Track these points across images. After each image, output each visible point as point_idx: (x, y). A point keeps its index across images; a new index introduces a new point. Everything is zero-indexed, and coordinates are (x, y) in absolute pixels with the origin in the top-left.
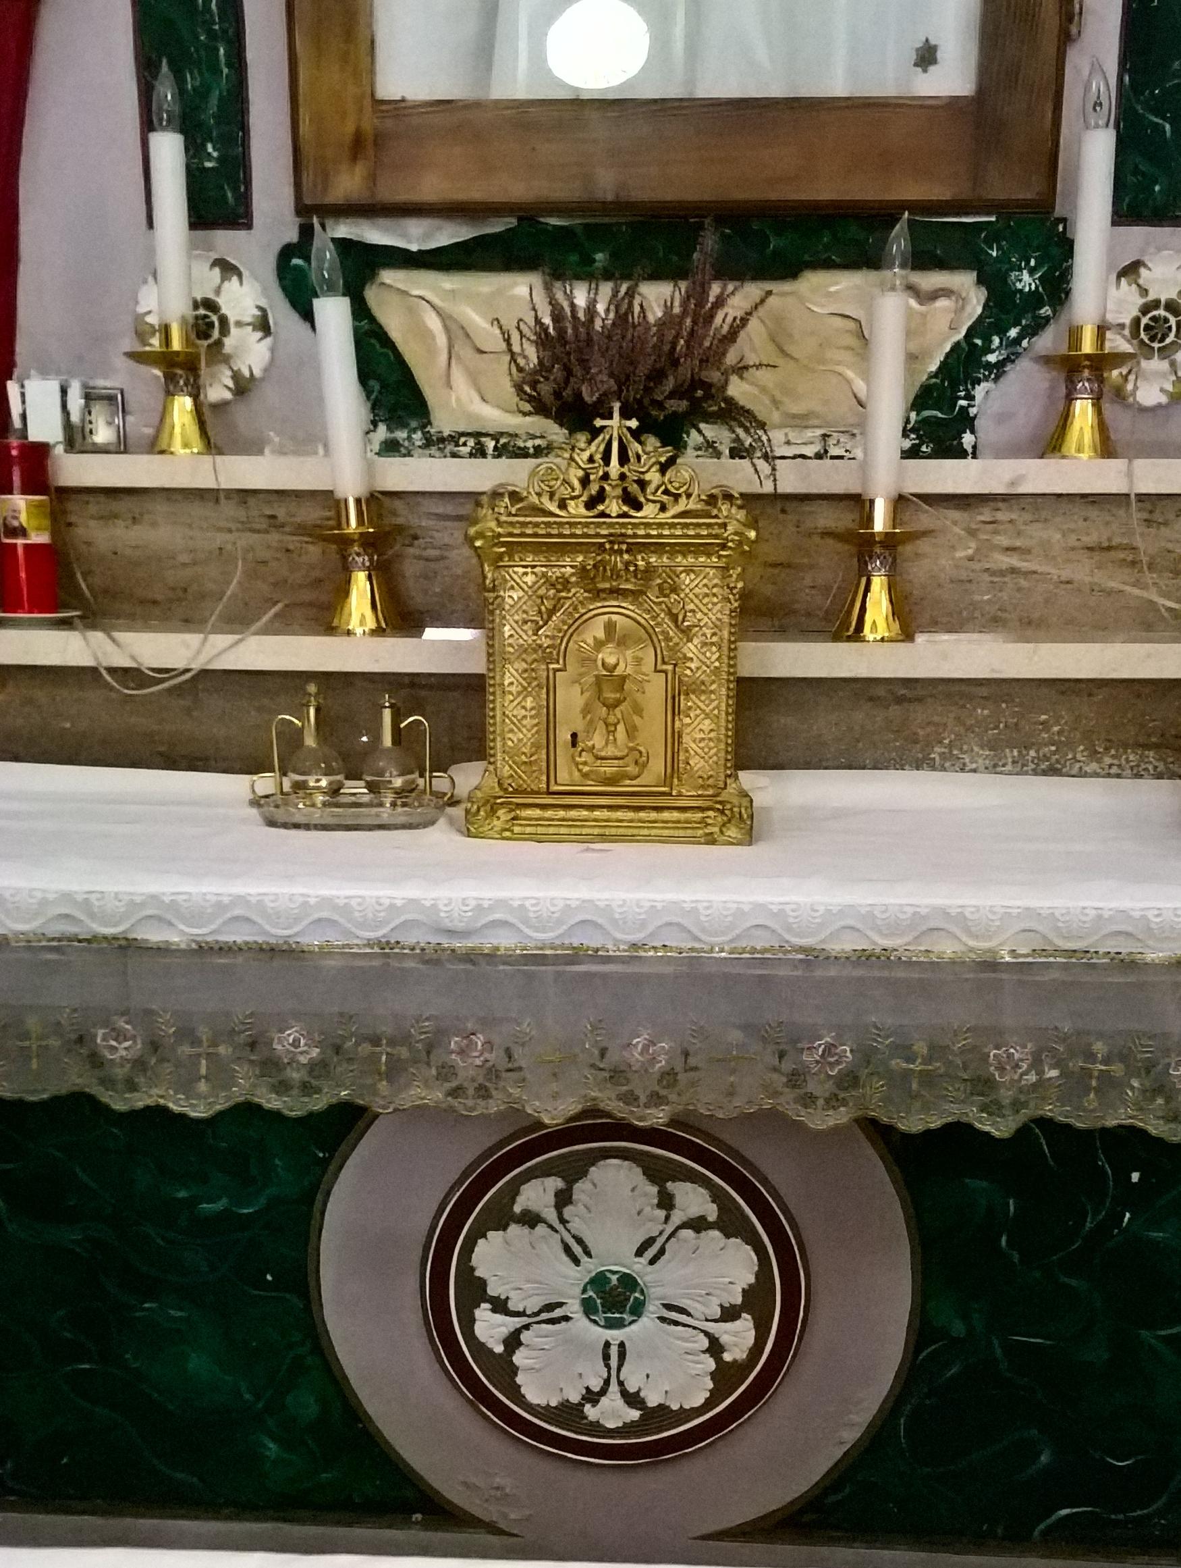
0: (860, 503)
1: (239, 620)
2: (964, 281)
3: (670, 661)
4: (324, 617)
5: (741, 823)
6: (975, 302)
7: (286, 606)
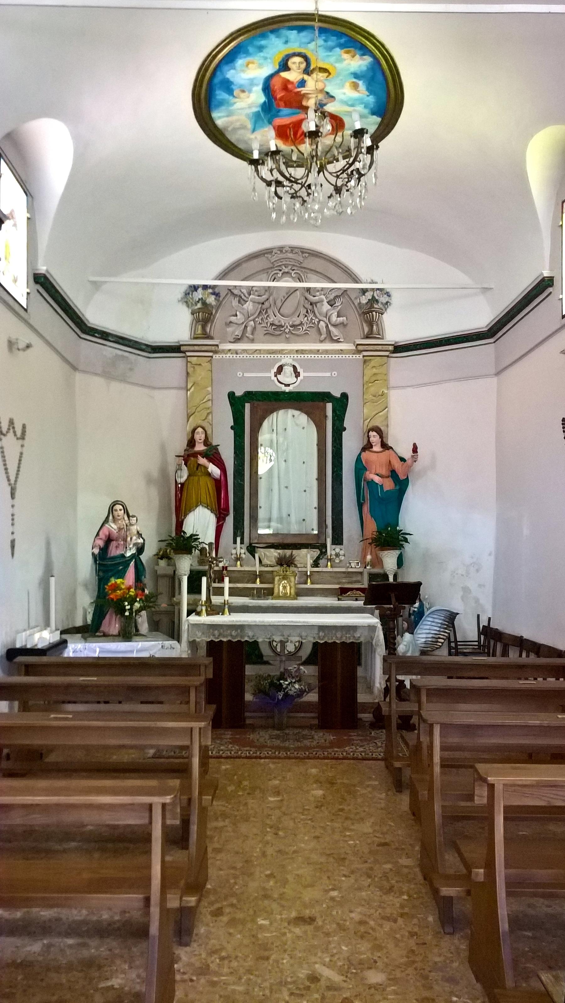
0: (386, 576)
1: (247, 582)
2: (318, 550)
3: (290, 585)
4: (254, 582)
5: (297, 599)
6: (319, 552)
7: (186, 464)
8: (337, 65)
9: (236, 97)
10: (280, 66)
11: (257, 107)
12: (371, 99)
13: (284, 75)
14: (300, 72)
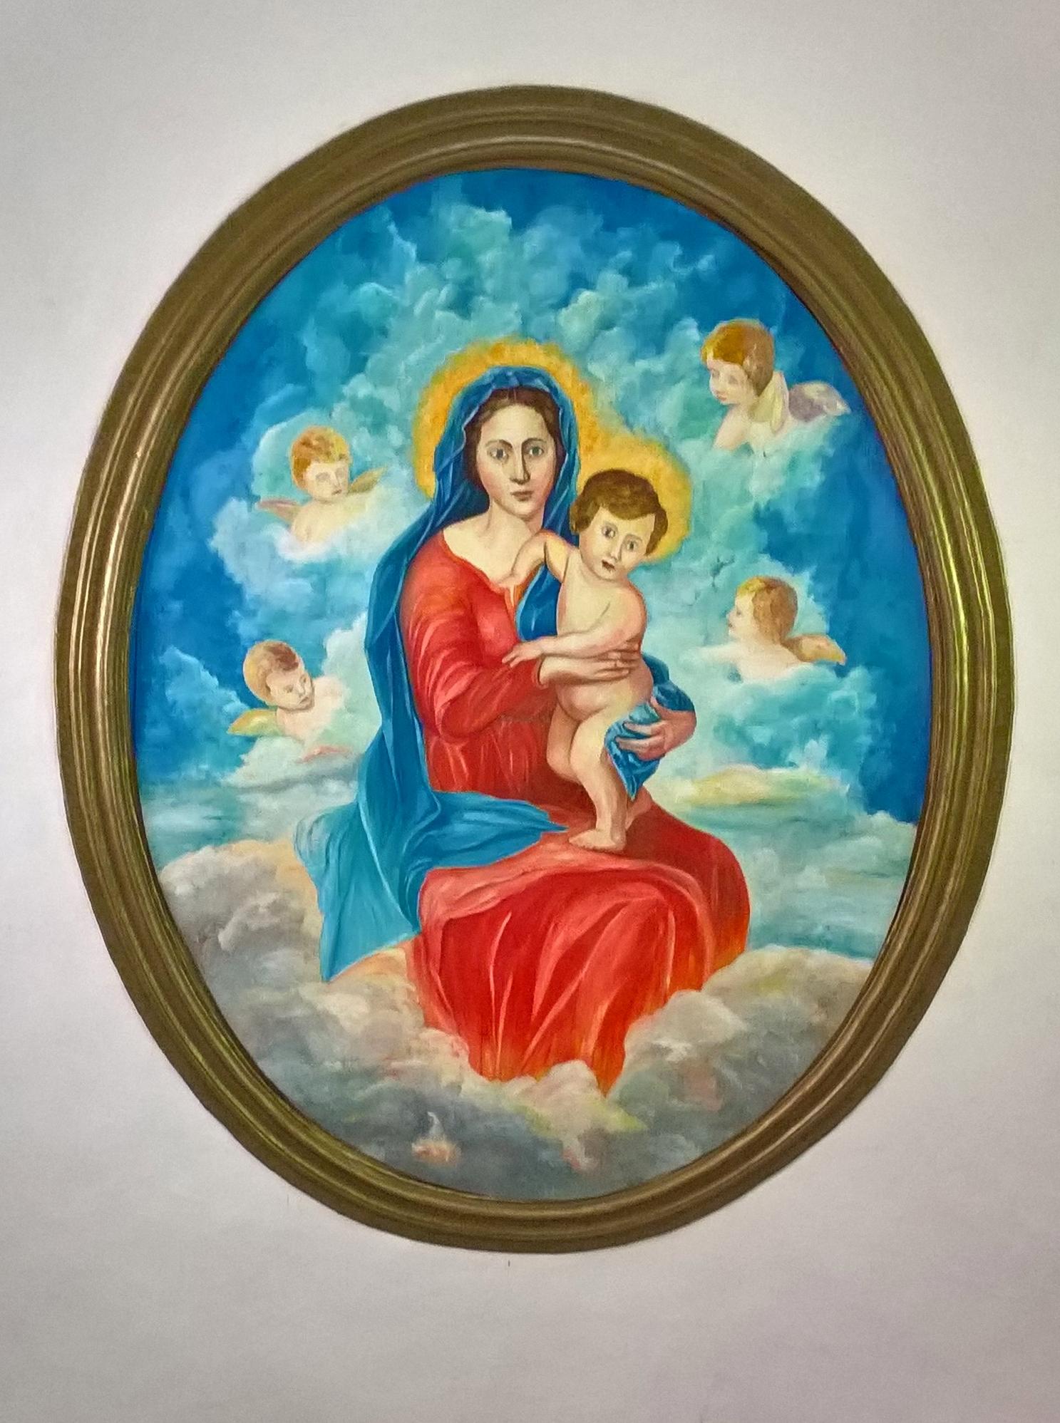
8: (689, 449)
9: (253, 702)
10: (441, 476)
11: (343, 776)
12: (855, 691)
13: (463, 539)
14: (527, 519)
